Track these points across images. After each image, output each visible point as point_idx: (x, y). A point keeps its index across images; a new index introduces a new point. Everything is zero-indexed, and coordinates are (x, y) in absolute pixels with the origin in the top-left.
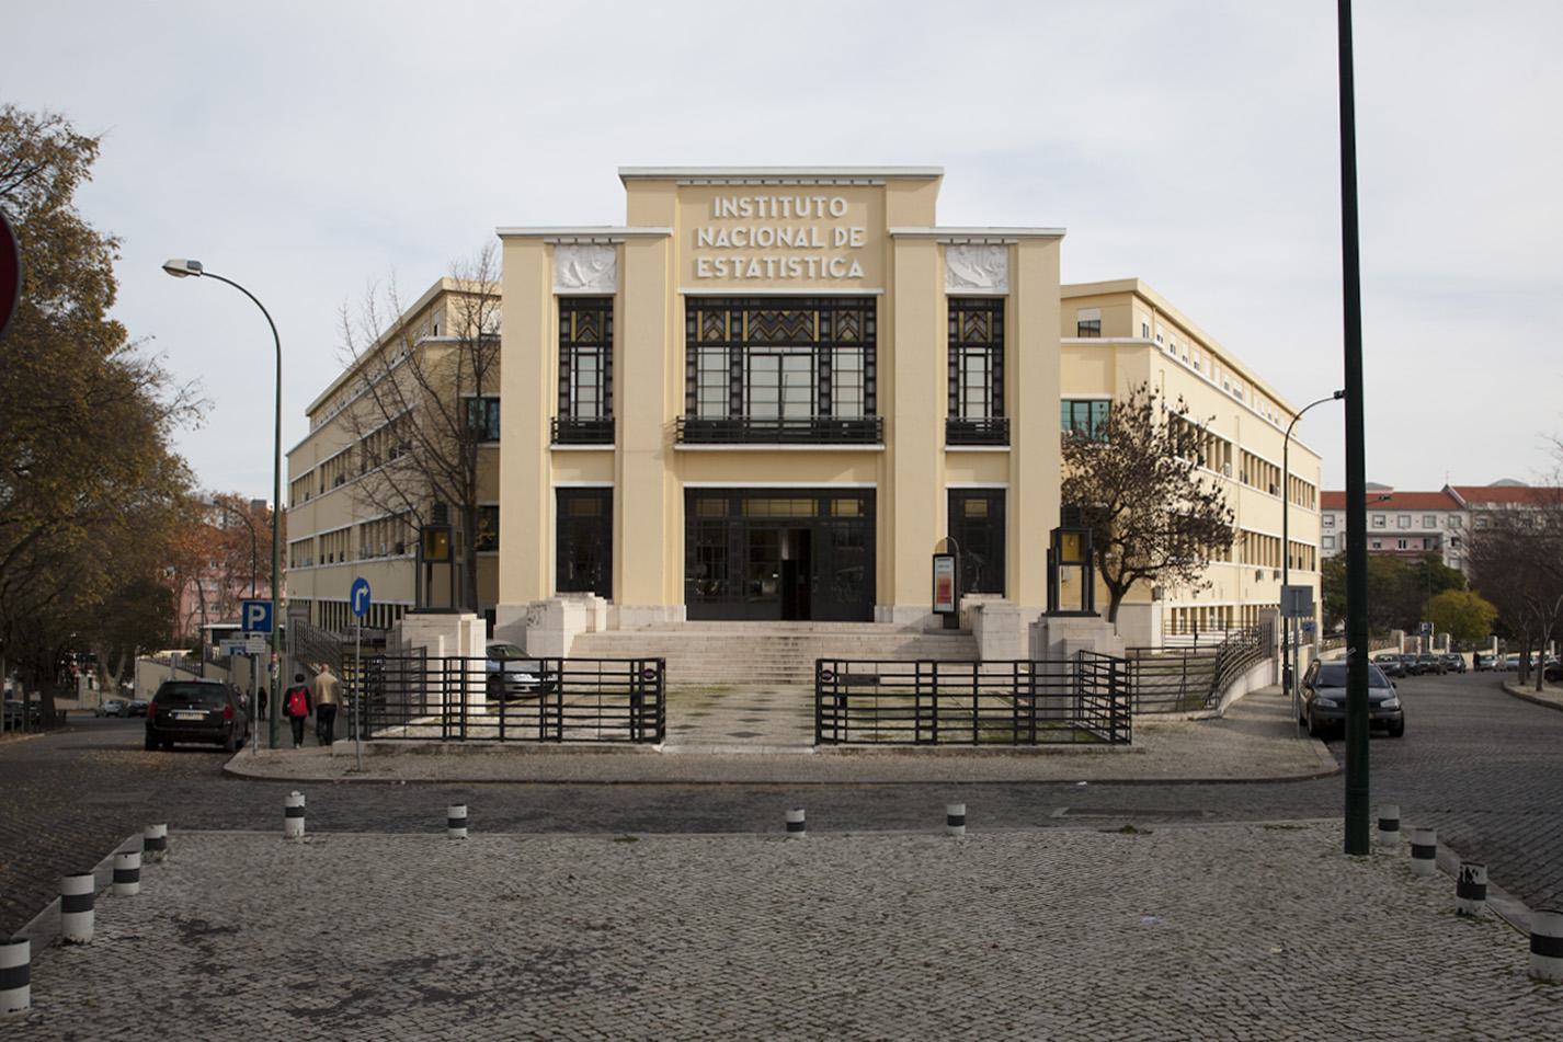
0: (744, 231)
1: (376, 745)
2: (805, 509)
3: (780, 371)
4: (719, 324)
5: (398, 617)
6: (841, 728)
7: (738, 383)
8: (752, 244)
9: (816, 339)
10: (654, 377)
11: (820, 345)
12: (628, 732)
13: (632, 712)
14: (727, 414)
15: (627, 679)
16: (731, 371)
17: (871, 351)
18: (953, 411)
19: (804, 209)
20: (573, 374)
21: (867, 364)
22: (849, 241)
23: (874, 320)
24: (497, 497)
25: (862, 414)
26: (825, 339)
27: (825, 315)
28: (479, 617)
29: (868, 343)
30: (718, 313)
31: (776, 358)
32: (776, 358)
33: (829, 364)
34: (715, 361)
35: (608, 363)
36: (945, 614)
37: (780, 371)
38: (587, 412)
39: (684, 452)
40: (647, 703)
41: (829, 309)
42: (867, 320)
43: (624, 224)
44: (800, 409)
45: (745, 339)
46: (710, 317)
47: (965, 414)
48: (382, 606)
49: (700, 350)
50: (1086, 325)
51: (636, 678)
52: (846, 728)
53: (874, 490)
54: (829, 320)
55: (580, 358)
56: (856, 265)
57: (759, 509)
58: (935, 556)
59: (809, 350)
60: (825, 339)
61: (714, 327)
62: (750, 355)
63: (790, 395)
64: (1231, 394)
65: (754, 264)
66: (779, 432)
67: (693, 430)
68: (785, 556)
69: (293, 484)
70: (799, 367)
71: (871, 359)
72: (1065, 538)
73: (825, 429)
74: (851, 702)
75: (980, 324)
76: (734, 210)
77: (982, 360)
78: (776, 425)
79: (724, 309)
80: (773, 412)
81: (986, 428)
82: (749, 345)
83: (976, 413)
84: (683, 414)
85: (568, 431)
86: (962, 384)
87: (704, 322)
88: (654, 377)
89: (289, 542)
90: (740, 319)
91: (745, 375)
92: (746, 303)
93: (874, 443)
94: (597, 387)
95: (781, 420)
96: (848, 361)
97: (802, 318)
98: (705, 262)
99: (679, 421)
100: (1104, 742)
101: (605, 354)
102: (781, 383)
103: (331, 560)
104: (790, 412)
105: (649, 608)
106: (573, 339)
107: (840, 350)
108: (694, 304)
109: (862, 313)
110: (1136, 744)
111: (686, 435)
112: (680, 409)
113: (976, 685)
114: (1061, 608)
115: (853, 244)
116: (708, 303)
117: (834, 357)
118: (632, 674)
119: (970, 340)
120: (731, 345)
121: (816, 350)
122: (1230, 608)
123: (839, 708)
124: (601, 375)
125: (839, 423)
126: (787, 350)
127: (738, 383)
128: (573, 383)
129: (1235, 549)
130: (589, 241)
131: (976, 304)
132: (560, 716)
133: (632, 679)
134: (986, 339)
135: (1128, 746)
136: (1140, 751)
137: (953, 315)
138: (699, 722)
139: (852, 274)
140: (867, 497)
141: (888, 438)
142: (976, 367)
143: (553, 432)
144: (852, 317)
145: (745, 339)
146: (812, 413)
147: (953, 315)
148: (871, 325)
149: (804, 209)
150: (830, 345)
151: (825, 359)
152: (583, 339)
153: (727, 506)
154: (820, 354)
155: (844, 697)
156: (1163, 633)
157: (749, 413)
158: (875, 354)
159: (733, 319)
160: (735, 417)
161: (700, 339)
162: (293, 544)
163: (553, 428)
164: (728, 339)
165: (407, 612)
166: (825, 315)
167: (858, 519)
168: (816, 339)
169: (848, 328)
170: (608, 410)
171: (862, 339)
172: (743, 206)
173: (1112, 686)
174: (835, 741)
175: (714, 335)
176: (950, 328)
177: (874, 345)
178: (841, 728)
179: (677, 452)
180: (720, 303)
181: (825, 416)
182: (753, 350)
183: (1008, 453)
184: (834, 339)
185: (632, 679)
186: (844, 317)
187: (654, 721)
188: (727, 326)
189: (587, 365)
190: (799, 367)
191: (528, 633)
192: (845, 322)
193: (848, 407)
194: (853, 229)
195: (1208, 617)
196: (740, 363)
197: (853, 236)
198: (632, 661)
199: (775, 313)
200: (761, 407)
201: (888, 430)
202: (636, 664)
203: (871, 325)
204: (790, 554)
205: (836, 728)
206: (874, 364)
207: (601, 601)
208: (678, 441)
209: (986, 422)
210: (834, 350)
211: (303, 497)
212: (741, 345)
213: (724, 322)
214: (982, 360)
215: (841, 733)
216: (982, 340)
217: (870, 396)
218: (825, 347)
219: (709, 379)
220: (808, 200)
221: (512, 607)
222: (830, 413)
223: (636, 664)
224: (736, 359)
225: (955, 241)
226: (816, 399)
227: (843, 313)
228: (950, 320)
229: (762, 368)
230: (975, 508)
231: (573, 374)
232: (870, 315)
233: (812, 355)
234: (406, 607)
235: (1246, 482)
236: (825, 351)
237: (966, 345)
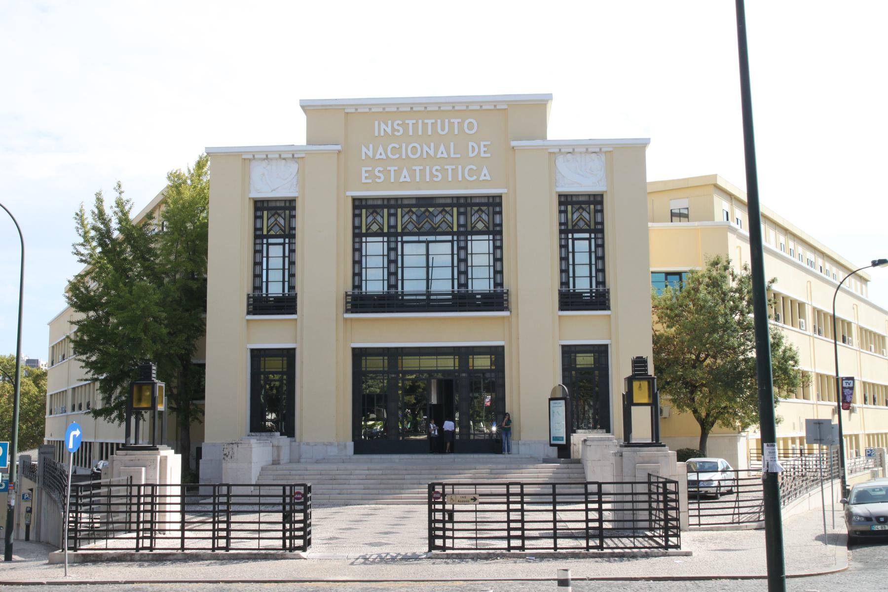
0: (397, 146)
1: (83, 555)
2: (449, 363)
3: (428, 255)
4: (379, 218)
5: (112, 454)
6: (449, 538)
7: (394, 266)
8: (404, 157)
9: (455, 229)
10: (323, 260)
11: (458, 234)
12: (280, 542)
13: (284, 526)
14: (386, 289)
15: (280, 500)
16: (388, 255)
17: (599, 235)
18: (564, 284)
19: (443, 130)
20: (265, 259)
21: (495, 248)
22: (479, 152)
23: (500, 213)
24: (204, 356)
25: (492, 288)
26: (462, 229)
27: (462, 210)
28: (176, 453)
29: (495, 231)
30: (378, 210)
31: (424, 245)
32: (424, 245)
33: (466, 248)
34: (375, 247)
35: (292, 251)
36: (560, 447)
37: (428, 255)
38: (275, 289)
39: (352, 319)
40: (296, 519)
41: (466, 205)
42: (495, 213)
43: (304, 143)
44: (443, 285)
45: (399, 230)
46: (372, 214)
47: (574, 286)
48: (107, 444)
49: (364, 239)
50: (678, 211)
51: (288, 500)
52: (453, 538)
53: (503, 347)
54: (465, 214)
55: (405, 245)
56: (485, 171)
57: (410, 363)
58: (550, 400)
59: (449, 238)
60: (462, 229)
61: (375, 221)
62: (574, 239)
63: (436, 273)
64: (805, 265)
65: (405, 172)
66: (428, 303)
67: (358, 302)
68: (434, 400)
69: (53, 347)
70: (442, 251)
71: (498, 243)
72: (636, 384)
73: (463, 301)
74: (457, 517)
75: (582, 215)
76: (389, 130)
77: (587, 242)
78: (424, 297)
79: (382, 207)
80: (421, 287)
81: (591, 296)
82: (403, 234)
83: (583, 284)
84: (349, 289)
85: (260, 304)
86: (571, 262)
87: (367, 218)
88: (323, 260)
89: (48, 394)
90: (395, 215)
91: (400, 258)
92: (399, 202)
93: (502, 310)
94: (284, 269)
95: (428, 294)
96: (480, 246)
97: (427, 214)
99: (347, 295)
100: (661, 547)
101: (289, 243)
102: (427, 264)
103: (80, 408)
104: (436, 287)
105: (324, 444)
106: (265, 232)
107: (474, 237)
108: (359, 204)
109: (491, 208)
110: (684, 549)
111: (353, 306)
112: (246, 287)
113: (183, 530)
114: (633, 441)
115: (482, 155)
116: (273, 204)
117: (469, 243)
118: (284, 496)
119: (576, 228)
120: (388, 235)
121: (593, 236)
122: (857, 436)
123: (448, 522)
124: (287, 259)
125: (473, 295)
127: (394, 266)
128: (265, 267)
129: (813, 389)
130: (277, 156)
131: (581, 199)
132: (228, 530)
133: (284, 500)
134: (589, 226)
135: (679, 550)
136: (688, 554)
137: (563, 208)
138: (347, 534)
139: (482, 178)
140: (497, 353)
141: (513, 305)
142: (582, 247)
143: (248, 305)
144: (483, 211)
145: (399, 230)
146: (453, 287)
147: (563, 208)
148: (497, 217)
149: (443, 130)
151: (462, 244)
152: (272, 233)
153: (386, 361)
154: (458, 241)
155: (451, 513)
156: (749, 459)
157: (402, 288)
158: (501, 240)
159: (389, 215)
160: (393, 291)
161: (364, 231)
162: (51, 395)
163: (248, 301)
164: (386, 230)
165: (118, 449)
166: (462, 210)
167: (490, 371)
168: (455, 229)
169: (480, 219)
170: (292, 288)
171: (592, 227)
172: (396, 127)
173: (665, 501)
174: (444, 548)
175: (375, 228)
176: (560, 218)
177: (500, 233)
178: (449, 538)
179: (346, 319)
180: (380, 202)
181: (463, 290)
182: (405, 238)
183: (609, 316)
184: (469, 229)
185: (284, 500)
186: (477, 212)
187: (301, 533)
188: (384, 220)
189: (276, 251)
190: (442, 251)
191: (224, 465)
192: (479, 215)
193: (481, 284)
194: (482, 143)
195: (790, 446)
196: (396, 249)
197: (483, 149)
198: (284, 486)
199: (423, 209)
200: (413, 284)
201: (512, 299)
202: (288, 488)
203: (599, 215)
204: (439, 398)
205: (444, 537)
206: (501, 248)
207: (285, 439)
208: (347, 311)
209: (591, 292)
210: (469, 238)
211: (60, 357)
212: (396, 234)
213: (383, 217)
214: (587, 242)
215: (449, 543)
216: (586, 227)
217: (499, 272)
218: (463, 234)
220: (447, 121)
221: (214, 445)
222: (397, 288)
223: (288, 488)
224: (393, 245)
225: (283, 156)
226: (456, 276)
227: (476, 208)
228: (560, 212)
229: (412, 252)
230: (584, 361)
231: (265, 259)
232: (498, 209)
234: (118, 444)
235: (819, 333)
236: (462, 238)
237: (574, 231)
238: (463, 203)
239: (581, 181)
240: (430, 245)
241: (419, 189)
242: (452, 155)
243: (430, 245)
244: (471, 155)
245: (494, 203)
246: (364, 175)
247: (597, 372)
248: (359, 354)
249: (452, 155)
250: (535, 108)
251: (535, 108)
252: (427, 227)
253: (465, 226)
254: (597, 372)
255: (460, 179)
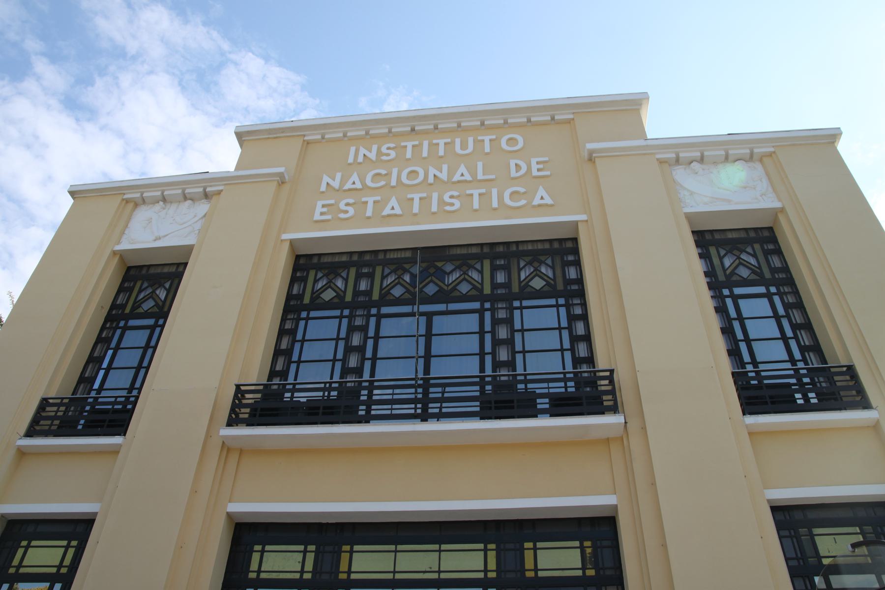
11: (494, 299)
29: (572, 294)
54: (506, 268)
61: (329, 285)
76: (372, 156)
82: (379, 304)
98: (538, 163)
115: (535, 173)
119: (734, 278)
126: (442, 307)
140: (598, 531)
141: (626, 395)
150: (509, 298)
175: (328, 295)
177: (581, 293)
182: (385, 310)
194: (534, 161)
212: (367, 306)
218: (503, 300)
219: (755, 329)
233: (735, 298)
237: (731, 285)
238: (503, 253)
239: (731, 193)
240: (435, 318)
241: (418, 224)
242: (480, 176)
243: (435, 318)
244: (514, 174)
245: (563, 250)
246: (319, 209)
247: (80, 427)
248: (247, 535)
249: (480, 176)
250: (629, 108)
251: (629, 108)
252: (431, 289)
253: (507, 285)
254: (80, 427)
255: (495, 204)
